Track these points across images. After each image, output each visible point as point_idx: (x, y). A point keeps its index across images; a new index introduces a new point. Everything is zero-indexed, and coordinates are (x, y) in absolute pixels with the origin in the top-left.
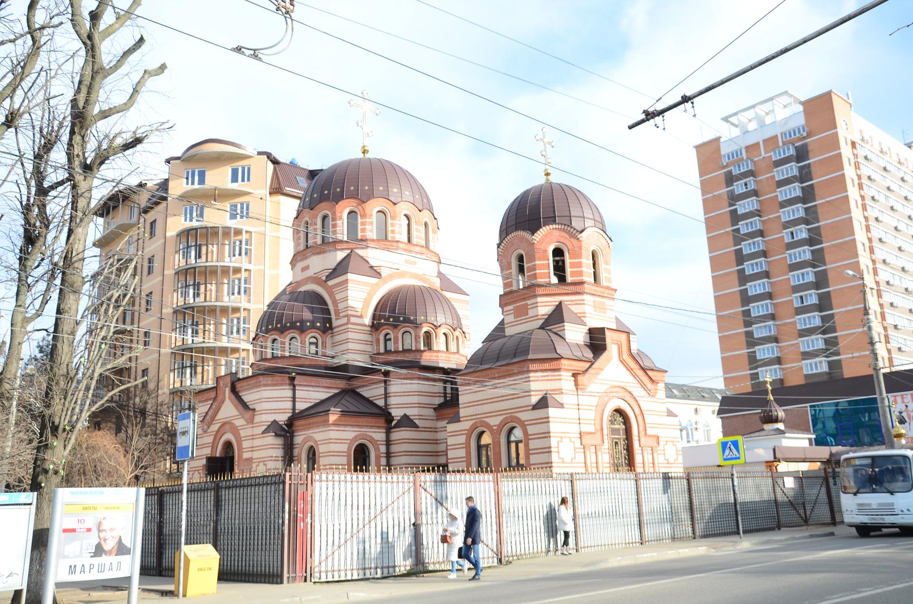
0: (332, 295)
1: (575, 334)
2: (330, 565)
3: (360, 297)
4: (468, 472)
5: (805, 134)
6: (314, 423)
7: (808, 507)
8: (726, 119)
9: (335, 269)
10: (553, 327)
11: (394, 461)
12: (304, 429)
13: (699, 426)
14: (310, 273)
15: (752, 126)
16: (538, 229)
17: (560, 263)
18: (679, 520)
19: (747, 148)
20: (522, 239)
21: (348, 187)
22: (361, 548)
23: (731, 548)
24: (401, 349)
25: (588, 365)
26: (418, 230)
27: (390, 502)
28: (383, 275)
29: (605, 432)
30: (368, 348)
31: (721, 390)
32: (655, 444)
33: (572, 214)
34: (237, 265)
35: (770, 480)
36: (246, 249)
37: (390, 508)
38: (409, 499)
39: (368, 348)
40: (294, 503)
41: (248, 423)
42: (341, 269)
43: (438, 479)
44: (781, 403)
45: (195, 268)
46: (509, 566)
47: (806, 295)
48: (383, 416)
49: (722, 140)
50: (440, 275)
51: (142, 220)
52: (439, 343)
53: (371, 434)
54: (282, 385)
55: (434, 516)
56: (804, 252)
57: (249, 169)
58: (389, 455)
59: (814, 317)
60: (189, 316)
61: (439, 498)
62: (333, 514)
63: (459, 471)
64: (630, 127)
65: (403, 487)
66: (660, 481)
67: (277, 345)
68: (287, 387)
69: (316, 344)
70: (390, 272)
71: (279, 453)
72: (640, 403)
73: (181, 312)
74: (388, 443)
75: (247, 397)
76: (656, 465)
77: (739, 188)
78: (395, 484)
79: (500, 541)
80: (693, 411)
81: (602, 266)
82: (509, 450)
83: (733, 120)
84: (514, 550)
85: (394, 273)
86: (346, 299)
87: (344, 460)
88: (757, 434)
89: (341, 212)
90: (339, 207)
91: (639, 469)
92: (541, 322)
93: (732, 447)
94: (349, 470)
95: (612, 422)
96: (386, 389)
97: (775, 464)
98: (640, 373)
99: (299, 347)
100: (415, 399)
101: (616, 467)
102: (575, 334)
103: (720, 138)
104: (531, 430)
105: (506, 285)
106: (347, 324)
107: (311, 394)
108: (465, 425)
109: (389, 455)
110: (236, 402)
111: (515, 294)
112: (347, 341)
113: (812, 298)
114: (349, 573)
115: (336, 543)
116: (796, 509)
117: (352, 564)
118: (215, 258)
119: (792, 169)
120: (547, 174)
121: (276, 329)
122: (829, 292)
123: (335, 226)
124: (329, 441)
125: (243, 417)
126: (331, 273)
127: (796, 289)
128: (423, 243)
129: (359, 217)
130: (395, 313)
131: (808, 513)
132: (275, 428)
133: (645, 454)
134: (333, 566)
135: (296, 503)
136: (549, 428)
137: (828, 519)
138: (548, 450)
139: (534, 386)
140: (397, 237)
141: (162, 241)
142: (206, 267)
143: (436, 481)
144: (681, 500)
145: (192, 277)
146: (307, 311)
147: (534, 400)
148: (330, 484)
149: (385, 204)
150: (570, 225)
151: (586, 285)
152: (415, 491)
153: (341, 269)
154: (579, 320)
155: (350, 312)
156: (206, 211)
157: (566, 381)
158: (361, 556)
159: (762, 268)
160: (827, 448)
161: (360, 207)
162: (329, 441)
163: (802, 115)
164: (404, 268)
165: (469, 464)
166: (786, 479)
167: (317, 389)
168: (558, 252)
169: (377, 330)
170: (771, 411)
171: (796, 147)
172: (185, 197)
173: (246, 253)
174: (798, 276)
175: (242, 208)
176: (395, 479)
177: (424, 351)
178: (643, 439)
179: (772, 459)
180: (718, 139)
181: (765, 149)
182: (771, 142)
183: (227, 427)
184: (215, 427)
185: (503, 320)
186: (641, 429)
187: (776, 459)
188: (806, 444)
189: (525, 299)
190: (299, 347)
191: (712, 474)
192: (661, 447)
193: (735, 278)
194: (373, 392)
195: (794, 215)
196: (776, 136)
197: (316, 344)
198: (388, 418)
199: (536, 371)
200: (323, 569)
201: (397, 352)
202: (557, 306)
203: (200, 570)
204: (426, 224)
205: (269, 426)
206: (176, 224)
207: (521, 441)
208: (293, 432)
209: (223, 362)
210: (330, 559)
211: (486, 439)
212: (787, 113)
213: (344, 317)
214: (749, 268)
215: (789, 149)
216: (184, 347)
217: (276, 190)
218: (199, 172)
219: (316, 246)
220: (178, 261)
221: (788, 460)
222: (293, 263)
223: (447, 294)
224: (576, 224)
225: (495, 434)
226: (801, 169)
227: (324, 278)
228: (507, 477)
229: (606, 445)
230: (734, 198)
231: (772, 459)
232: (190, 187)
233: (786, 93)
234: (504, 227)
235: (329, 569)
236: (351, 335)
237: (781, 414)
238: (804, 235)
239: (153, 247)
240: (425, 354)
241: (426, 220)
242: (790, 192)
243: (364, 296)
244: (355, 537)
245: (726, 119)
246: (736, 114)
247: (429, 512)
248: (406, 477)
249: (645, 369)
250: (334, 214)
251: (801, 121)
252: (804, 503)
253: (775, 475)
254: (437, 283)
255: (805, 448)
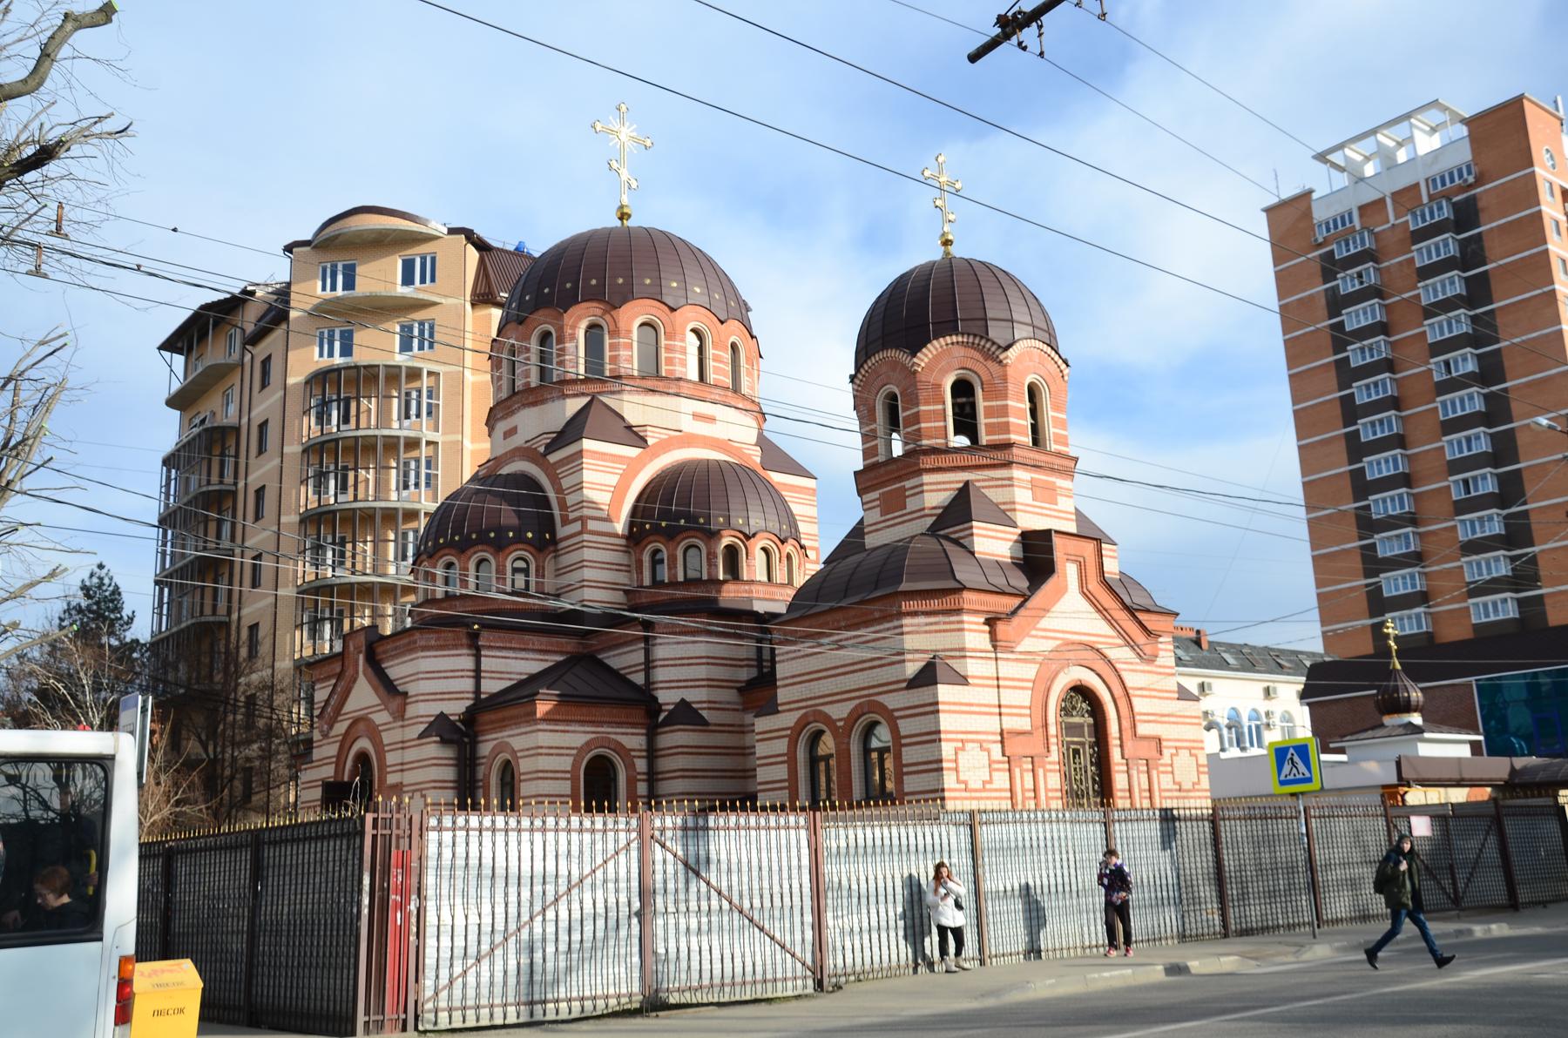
0: (555, 481)
1: (993, 543)
2: (457, 993)
3: (608, 481)
4: (794, 809)
5: (1471, 179)
6: (512, 718)
7: (1461, 877)
8: (1322, 157)
9: (561, 433)
10: (954, 531)
11: (665, 787)
12: (494, 730)
13: (1276, 720)
14: (518, 441)
15: (1369, 170)
16: (924, 345)
17: (968, 409)
18: (1196, 901)
19: (1362, 209)
20: (895, 364)
21: (587, 280)
22: (525, 961)
23: (1291, 958)
24: (681, 578)
25: (1017, 601)
26: (717, 359)
27: (587, 870)
28: (650, 441)
29: (1052, 730)
30: (622, 578)
31: (1314, 654)
32: (1155, 754)
33: (990, 315)
34: (412, 434)
35: (1381, 822)
36: (429, 405)
37: (588, 881)
38: (627, 865)
39: (622, 578)
40: (382, 872)
41: (395, 719)
42: (572, 431)
43: (690, 824)
44: (1416, 675)
45: (336, 440)
46: (838, 994)
47: (1475, 478)
48: (639, 703)
49: (1315, 196)
50: (762, 442)
51: (248, 357)
52: (754, 566)
53: (619, 738)
54: (455, 647)
55: (682, 896)
56: (1471, 397)
57: (433, 260)
58: (652, 777)
59: (1490, 518)
60: (326, 527)
61: (692, 861)
62: (466, 895)
63: (774, 808)
64: (973, 58)
65: (616, 841)
66: (1156, 826)
67: (455, 573)
68: (465, 651)
69: (526, 572)
70: (664, 435)
71: (449, 773)
72: (1124, 675)
73: (316, 520)
74: (652, 753)
75: (397, 670)
76: (1156, 794)
77: (1346, 283)
78: (599, 836)
79: (819, 944)
80: (1261, 694)
81: (1049, 413)
82: (869, 766)
83: (1336, 158)
84: (849, 961)
85: (671, 438)
86: (579, 487)
87: (566, 787)
88: (1370, 733)
89: (574, 327)
90: (569, 318)
91: (1121, 802)
92: (930, 521)
93: (1296, 758)
94: (576, 809)
95: (1066, 711)
96: (647, 653)
97: (1402, 790)
98: (1122, 616)
99: (494, 579)
100: (701, 672)
101: (1074, 796)
102: (993, 543)
103: (1310, 192)
104: (906, 727)
105: (867, 454)
106: (580, 533)
107: (507, 666)
108: (787, 719)
109: (652, 777)
110: (376, 681)
111: (882, 470)
112: (580, 565)
113: (1487, 484)
114: (498, 1012)
115: (472, 950)
116: (1435, 878)
117: (505, 994)
118: (373, 422)
119: (1447, 245)
120: (947, 243)
121: (451, 545)
122: (1519, 470)
123: (563, 351)
124: (536, 751)
125: (386, 708)
126: (554, 440)
127: (1456, 467)
128: (728, 381)
129: (607, 337)
130: (681, 508)
131: (1461, 885)
132: (441, 728)
133: (1134, 773)
134: (464, 997)
135: (386, 872)
136: (937, 723)
137: (1502, 898)
138: (936, 766)
139: (910, 642)
140: (678, 371)
141: (281, 393)
142: (356, 438)
143: (685, 829)
144: (1199, 863)
145: (333, 457)
146: (515, 510)
147: (911, 669)
148: (461, 834)
149: (653, 311)
150: (984, 335)
151: (1015, 450)
152: (641, 849)
153: (572, 431)
154: (1003, 516)
155: (586, 512)
156: (359, 337)
157: (975, 636)
158: (524, 978)
159: (1390, 429)
160: (1506, 760)
161: (607, 317)
162: (536, 751)
163: (1466, 145)
164: (690, 426)
165: (794, 796)
166: (1414, 820)
167: (523, 655)
168: (963, 389)
169: (637, 544)
170: (1396, 689)
171: (1455, 205)
172: (322, 311)
173: (429, 413)
174: (1459, 443)
175: (422, 332)
176: (599, 826)
177: (725, 581)
178: (1128, 744)
179: (1393, 780)
180: (1307, 194)
181: (1395, 210)
182: (1407, 197)
183: (361, 726)
184: (341, 728)
185: (861, 522)
186: (1126, 724)
187: (1403, 782)
188: (1465, 751)
189: (900, 478)
190: (494, 579)
191: (1260, 812)
192: (1166, 759)
193: (1341, 449)
194: (626, 660)
195: (1450, 331)
196: (1417, 185)
197: (526, 572)
198: (653, 707)
199: (915, 614)
200: (443, 1004)
201: (674, 584)
202: (960, 490)
203: (158, 1013)
204: (734, 347)
205: (431, 724)
206: (306, 359)
207: (887, 749)
208: (476, 735)
209: (390, 611)
210: (458, 983)
211: (827, 745)
212: (1435, 142)
213: (575, 520)
214: (1367, 430)
215: (1440, 208)
216: (318, 583)
217: (483, 298)
218: (345, 267)
219: (528, 390)
220: (309, 428)
221: (1426, 783)
222: (492, 420)
223: (776, 477)
224: (996, 332)
225: (842, 735)
226: (1463, 244)
227: (542, 449)
228: (835, 819)
229: (1054, 756)
230: (1336, 303)
231: (1393, 780)
232: (328, 294)
233: (1435, 104)
234: (863, 343)
235: (457, 1004)
236: (588, 554)
237: (1416, 695)
238: (1471, 366)
239: (265, 405)
240: (726, 587)
241: (733, 339)
242: (1443, 286)
243: (613, 480)
244: (512, 940)
245: (1322, 157)
246: (1341, 147)
247: (671, 886)
248: (622, 820)
249: (1129, 605)
250: (560, 330)
251: (1465, 155)
252: (1451, 867)
253: (1392, 812)
254: (755, 456)
255: (1459, 760)
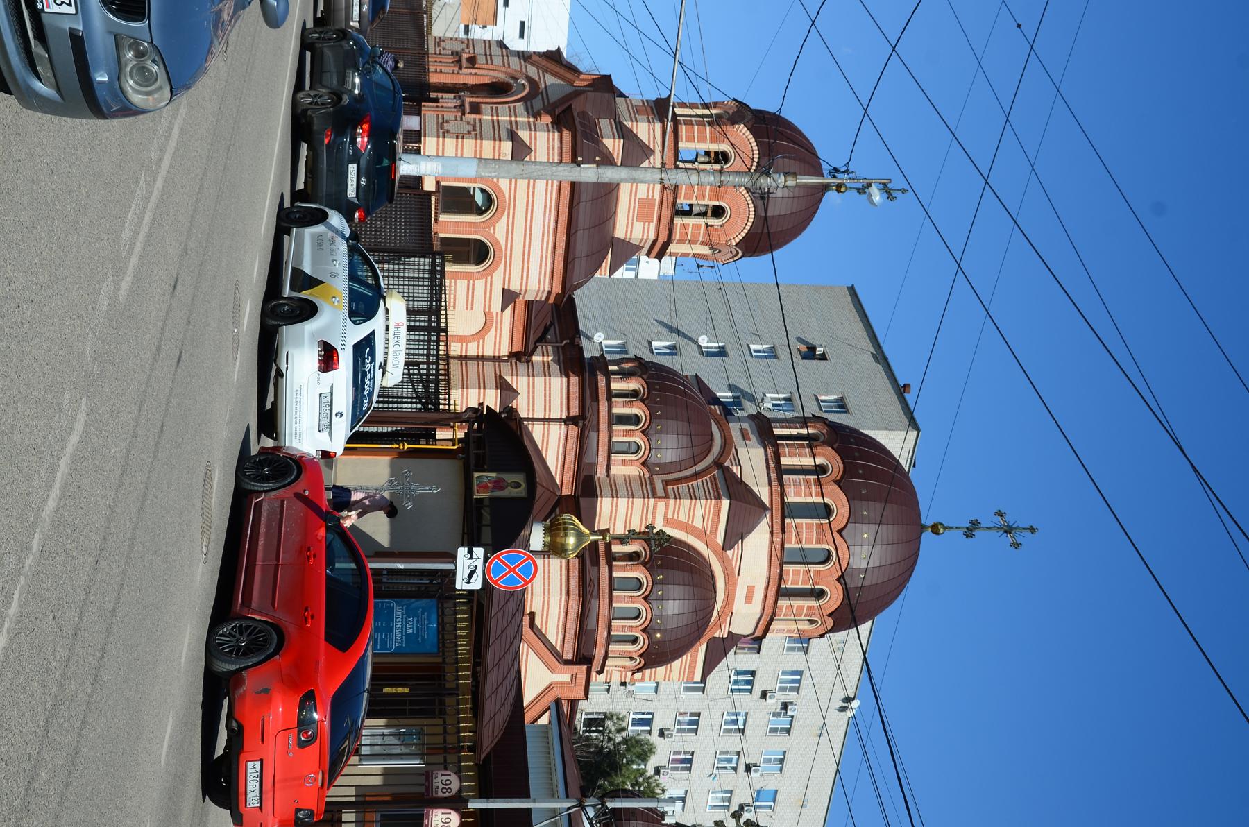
28: (729, 553)
74: (480, 359)
86: (693, 496)
153: (737, 491)
243: (698, 523)
